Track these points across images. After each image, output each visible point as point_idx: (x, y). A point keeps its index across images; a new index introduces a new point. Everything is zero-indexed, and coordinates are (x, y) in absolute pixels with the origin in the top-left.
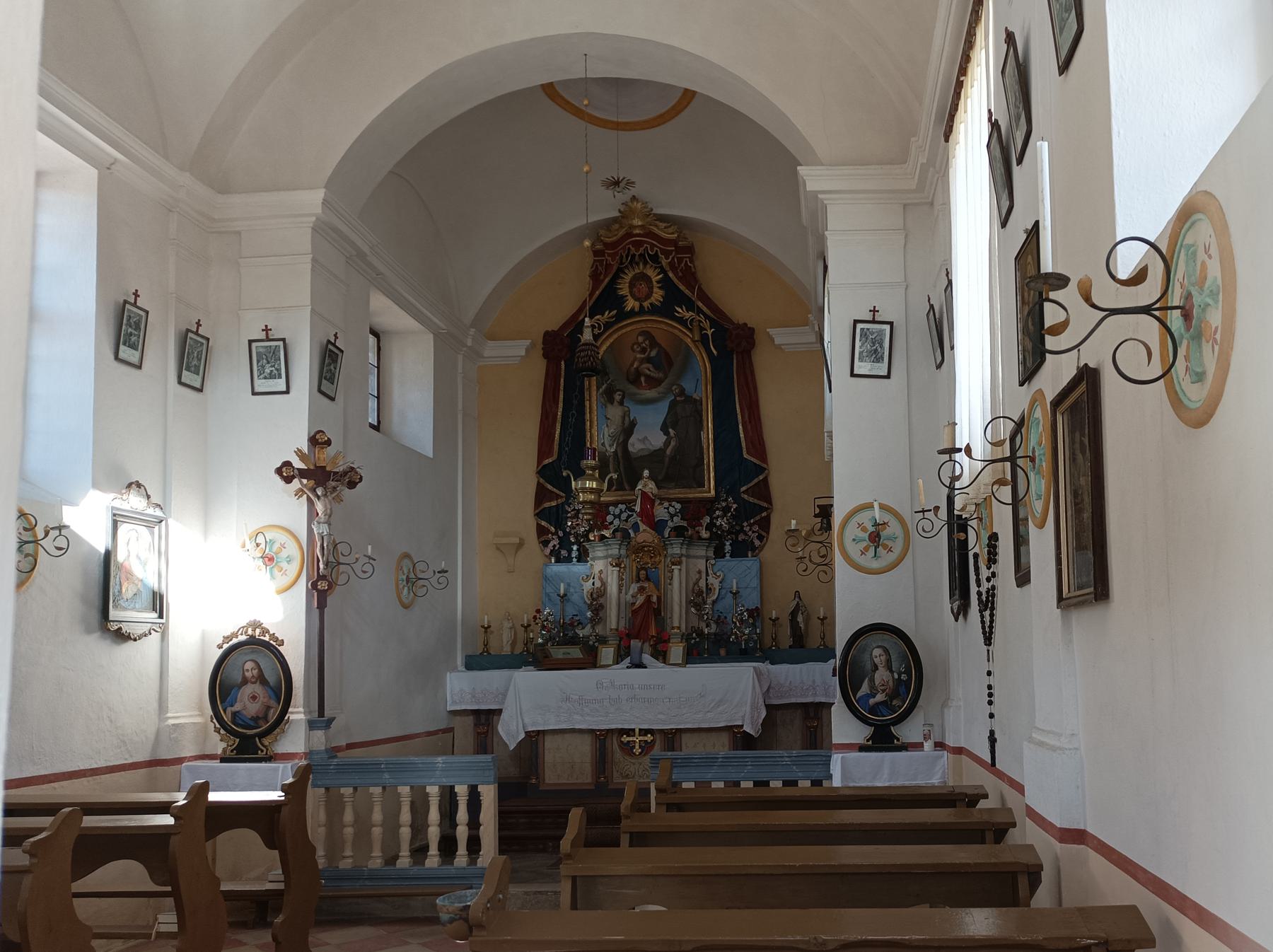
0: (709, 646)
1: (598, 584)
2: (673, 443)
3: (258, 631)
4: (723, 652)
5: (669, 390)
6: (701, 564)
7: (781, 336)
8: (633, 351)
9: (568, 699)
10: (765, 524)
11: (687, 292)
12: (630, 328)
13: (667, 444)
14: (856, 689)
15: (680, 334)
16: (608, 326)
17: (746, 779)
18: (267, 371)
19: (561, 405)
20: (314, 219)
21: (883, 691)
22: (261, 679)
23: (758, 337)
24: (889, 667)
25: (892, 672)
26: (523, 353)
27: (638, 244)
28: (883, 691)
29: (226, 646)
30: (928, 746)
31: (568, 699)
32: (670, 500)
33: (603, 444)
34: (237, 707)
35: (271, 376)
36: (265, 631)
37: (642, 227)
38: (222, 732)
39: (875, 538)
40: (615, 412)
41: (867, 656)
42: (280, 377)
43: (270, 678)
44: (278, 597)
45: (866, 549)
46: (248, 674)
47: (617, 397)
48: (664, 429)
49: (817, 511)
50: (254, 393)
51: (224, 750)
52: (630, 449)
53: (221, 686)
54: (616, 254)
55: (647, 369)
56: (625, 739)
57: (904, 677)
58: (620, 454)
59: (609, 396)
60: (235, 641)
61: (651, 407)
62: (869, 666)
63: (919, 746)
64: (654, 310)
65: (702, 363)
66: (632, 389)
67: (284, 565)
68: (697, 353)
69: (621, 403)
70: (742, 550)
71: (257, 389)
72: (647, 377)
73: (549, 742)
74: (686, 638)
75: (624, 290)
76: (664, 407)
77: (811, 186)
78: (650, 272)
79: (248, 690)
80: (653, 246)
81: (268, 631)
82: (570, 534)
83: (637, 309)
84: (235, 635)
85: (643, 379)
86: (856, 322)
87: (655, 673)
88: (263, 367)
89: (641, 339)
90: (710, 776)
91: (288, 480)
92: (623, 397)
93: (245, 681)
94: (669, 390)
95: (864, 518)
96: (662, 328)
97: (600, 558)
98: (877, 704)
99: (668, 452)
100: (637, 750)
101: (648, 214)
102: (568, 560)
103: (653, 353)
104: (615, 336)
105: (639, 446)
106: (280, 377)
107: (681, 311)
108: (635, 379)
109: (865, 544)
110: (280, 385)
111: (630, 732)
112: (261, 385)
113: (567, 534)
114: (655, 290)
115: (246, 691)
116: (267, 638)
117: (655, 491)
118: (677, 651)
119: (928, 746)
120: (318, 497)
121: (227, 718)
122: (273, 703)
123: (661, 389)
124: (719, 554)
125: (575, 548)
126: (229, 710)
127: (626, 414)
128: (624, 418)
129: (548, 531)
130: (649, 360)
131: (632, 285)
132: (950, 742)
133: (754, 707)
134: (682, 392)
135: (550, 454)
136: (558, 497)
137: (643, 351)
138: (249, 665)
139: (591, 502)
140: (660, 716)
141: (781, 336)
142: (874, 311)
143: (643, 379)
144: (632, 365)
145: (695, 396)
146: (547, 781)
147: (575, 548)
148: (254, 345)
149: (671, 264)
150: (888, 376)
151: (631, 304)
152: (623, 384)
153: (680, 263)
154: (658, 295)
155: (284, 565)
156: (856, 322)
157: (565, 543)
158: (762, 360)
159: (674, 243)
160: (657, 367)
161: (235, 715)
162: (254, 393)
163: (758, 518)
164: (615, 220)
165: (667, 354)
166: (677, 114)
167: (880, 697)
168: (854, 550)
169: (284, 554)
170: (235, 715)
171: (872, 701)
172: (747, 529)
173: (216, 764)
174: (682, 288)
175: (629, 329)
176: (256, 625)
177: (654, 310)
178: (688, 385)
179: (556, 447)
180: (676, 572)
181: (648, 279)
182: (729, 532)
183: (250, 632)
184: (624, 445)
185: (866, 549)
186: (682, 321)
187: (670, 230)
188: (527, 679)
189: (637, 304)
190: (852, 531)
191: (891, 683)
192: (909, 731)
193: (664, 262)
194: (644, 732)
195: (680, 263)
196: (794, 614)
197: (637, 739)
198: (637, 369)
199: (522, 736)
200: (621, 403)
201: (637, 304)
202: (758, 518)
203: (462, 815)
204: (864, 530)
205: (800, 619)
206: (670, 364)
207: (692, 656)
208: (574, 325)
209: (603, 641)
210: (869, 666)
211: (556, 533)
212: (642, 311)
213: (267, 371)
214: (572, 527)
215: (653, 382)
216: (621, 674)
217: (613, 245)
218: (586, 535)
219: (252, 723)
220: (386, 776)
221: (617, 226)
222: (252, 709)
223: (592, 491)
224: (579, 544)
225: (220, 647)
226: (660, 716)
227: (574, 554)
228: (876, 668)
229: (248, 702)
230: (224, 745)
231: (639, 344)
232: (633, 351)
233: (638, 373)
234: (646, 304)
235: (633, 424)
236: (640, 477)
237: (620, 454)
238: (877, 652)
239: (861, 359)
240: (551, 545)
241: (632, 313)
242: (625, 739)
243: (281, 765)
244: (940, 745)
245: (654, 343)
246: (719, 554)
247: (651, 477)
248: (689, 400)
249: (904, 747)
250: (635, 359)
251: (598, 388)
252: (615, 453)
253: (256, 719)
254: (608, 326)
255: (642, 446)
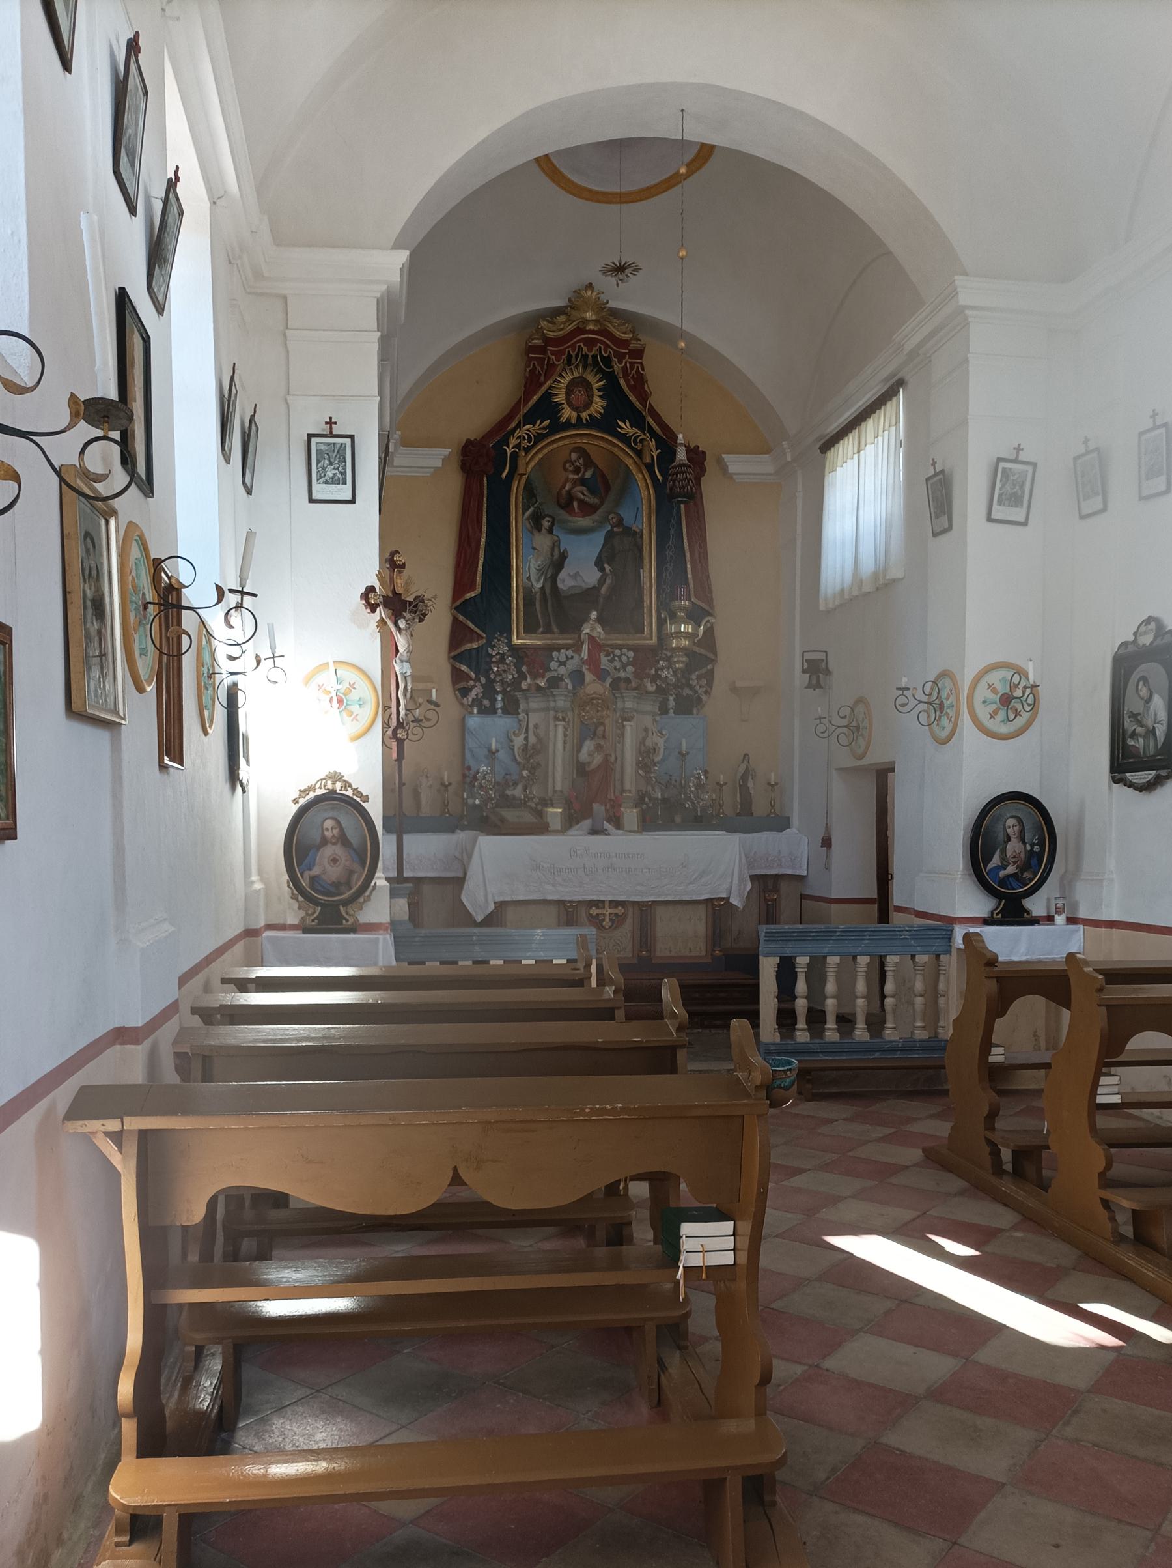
0: (669, 811)
1: (532, 740)
2: (608, 581)
3: (338, 785)
4: (678, 819)
5: (606, 519)
6: (648, 721)
7: (736, 464)
8: (565, 470)
9: (538, 867)
10: (710, 676)
11: (637, 404)
12: (562, 442)
13: (602, 581)
14: (988, 860)
15: (615, 450)
16: (539, 438)
17: (862, 954)
18: (330, 473)
19: (484, 528)
20: (384, 287)
21: (1015, 863)
22: (343, 839)
23: (709, 463)
24: (1022, 839)
25: (1024, 843)
26: (440, 464)
27: (590, 343)
28: (1015, 863)
29: (302, 801)
30: (1060, 920)
31: (538, 867)
32: (620, 647)
33: (529, 578)
34: (316, 871)
35: (334, 481)
36: (347, 785)
37: (596, 322)
38: (301, 898)
39: (1006, 700)
40: (543, 541)
41: (1000, 827)
42: (345, 483)
43: (353, 836)
44: (353, 745)
45: (996, 712)
46: (328, 834)
47: (546, 523)
48: (599, 563)
49: (806, 665)
50: (311, 500)
51: (303, 920)
52: (560, 585)
53: (299, 844)
54: (562, 352)
55: (580, 492)
56: (594, 911)
57: (1036, 849)
58: (548, 591)
59: (536, 521)
60: (312, 795)
61: (584, 538)
62: (1001, 837)
63: (1050, 919)
64: (593, 423)
65: (644, 489)
66: (563, 514)
67: (355, 708)
68: (639, 477)
69: (550, 531)
70: (688, 706)
71: (315, 496)
72: (581, 502)
73: (660, 911)
74: (640, 800)
75: (560, 398)
76: (599, 538)
77: (964, 299)
78: (590, 377)
79: (328, 851)
80: (607, 346)
81: (350, 786)
82: (494, 681)
83: (574, 421)
84: (311, 788)
85: (575, 504)
86: (310, 436)
87: (616, 843)
88: (324, 468)
89: (574, 456)
90: (826, 950)
91: (373, 608)
92: (553, 524)
93: (324, 842)
94: (606, 519)
95: (996, 677)
96: (598, 443)
97: (535, 711)
98: (1008, 876)
99: (603, 590)
100: (607, 923)
101: (601, 307)
102: (492, 711)
103: (588, 475)
104: (545, 451)
105: (570, 583)
106: (345, 483)
107: (625, 427)
108: (566, 503)
109: (994, 707)
110: (345, 492)
111: (598, 904)
112: (320, 490)
113: (491, 682)
114: (596, 399)
115: (325, 850)
116: (350, 793)
117: (603, 636)
118: (630, 815)
119: (1060, 920)
120: (399, 630)
121: (305, 883)
122: (356, 867)
123: (596, 517)
124: (664, 711)
125: (499, 698)
126: (307, 874)
127: (556, 544)
128: (553, 549)
129: (468, 677)
130: (583, 482)
131: (569, 391)
132: (1082, 914)
133: (741, 880)
134: (620, 522)
135: (472, 588)
136: (480, 637)
137: (577, 470)
138: (329, 824)
139: (685, 649)
140: (639, 888)
141: (736, 464)
142: (331, 423)
143: (575, 504)
144: (564, 486)
145: (634, 528)
146: (658, 954)
147: (499, 698)
148: (314, 440)
149: (624, 369)
150: (1025, 524)
151: (567, 413)
152: (553, 509)
153: (632, 368)
154: (598, 405)
155: (355, 708)
156: (310, 436)
157: (490, 692)
158: (710, 487)
159: (625, 343)
160: (592, 492)
161: (313, 880)
162: (311, 500)
163: (704, 671)
164: (557, 312)
165: (603, 476)
166: (668, 189)
167: (1011, 870)
168: (983, 713)
169: (355, 696)
170: (313, 880)
171: (1002, 873)
172: (694, 683)
173: (299, 935)
174: (633, 399)
175: (561, 443)
176: (335, 777)
177: (593, 423)
178: (627, 515)
179: (479, 579)
180: (628, 729)
181: (587, 386)
182: (675, 686)
183: (330, 786)
184: (554, 579)
185: (996, 712)
186: (624, 438)
187: (624, 328)
188: (489, 846)
189: (574, 414)
190: (982, 692)
191: (1023, 855)
192: (1036, 905)
193: (617, 367)
194: (615, 904)
195: (632, 368)
196: (745, 777)
197: (608, 911)
198: (569, 492)
199: (492, 907)
200: (550, 531)
201: (574, 414)
202: (704, 671)
203: (801, 987)
204: (995, 691)
205: (750, 784)
206: (607, 487)
207: (648, 823)
208: (501, 430)
209: (547, 802)
210: (1001, 837)
211: (477, 680)
212: (579, 423)
213: (330, 473)
214: (498, 674)
215: (588, 509)
216: (578, 839)
217: (559, 341)
218: (516, 683)
219: (332, 889)
220: (477, 948)
221: (563, 318)
222: (333, 873)
223: (686, 635)
224: (504, 692)
225: (295, 801)
226: (639, 888)
227: (499, 705)
228: (1009, 839)
229: (329, 864)
230: (302, 913)
231: (572, 463)
232: (565, 470)
233: (571, 498)
234: (584, 415)
235: (563, 557)
236: (586, 619)
237: (548, 591)
238: (1011, 822)
239: (1000, 503)
240: (474, 692)
241: (568, 425)
242: (594, 911)
243: (381, 937)
244: (1071, 920)
245: (589, 463)
246: (664, 711)
247: (599, 620)
248: (628, 531)
249: (1035, 921)
250: (567, 480)
251: (523, 514)
252: (542, 588)
253: (337, 885)
254: (539, 438)
255: (573, 583)
